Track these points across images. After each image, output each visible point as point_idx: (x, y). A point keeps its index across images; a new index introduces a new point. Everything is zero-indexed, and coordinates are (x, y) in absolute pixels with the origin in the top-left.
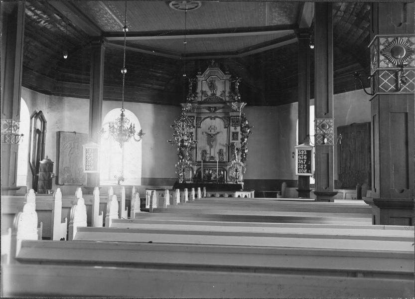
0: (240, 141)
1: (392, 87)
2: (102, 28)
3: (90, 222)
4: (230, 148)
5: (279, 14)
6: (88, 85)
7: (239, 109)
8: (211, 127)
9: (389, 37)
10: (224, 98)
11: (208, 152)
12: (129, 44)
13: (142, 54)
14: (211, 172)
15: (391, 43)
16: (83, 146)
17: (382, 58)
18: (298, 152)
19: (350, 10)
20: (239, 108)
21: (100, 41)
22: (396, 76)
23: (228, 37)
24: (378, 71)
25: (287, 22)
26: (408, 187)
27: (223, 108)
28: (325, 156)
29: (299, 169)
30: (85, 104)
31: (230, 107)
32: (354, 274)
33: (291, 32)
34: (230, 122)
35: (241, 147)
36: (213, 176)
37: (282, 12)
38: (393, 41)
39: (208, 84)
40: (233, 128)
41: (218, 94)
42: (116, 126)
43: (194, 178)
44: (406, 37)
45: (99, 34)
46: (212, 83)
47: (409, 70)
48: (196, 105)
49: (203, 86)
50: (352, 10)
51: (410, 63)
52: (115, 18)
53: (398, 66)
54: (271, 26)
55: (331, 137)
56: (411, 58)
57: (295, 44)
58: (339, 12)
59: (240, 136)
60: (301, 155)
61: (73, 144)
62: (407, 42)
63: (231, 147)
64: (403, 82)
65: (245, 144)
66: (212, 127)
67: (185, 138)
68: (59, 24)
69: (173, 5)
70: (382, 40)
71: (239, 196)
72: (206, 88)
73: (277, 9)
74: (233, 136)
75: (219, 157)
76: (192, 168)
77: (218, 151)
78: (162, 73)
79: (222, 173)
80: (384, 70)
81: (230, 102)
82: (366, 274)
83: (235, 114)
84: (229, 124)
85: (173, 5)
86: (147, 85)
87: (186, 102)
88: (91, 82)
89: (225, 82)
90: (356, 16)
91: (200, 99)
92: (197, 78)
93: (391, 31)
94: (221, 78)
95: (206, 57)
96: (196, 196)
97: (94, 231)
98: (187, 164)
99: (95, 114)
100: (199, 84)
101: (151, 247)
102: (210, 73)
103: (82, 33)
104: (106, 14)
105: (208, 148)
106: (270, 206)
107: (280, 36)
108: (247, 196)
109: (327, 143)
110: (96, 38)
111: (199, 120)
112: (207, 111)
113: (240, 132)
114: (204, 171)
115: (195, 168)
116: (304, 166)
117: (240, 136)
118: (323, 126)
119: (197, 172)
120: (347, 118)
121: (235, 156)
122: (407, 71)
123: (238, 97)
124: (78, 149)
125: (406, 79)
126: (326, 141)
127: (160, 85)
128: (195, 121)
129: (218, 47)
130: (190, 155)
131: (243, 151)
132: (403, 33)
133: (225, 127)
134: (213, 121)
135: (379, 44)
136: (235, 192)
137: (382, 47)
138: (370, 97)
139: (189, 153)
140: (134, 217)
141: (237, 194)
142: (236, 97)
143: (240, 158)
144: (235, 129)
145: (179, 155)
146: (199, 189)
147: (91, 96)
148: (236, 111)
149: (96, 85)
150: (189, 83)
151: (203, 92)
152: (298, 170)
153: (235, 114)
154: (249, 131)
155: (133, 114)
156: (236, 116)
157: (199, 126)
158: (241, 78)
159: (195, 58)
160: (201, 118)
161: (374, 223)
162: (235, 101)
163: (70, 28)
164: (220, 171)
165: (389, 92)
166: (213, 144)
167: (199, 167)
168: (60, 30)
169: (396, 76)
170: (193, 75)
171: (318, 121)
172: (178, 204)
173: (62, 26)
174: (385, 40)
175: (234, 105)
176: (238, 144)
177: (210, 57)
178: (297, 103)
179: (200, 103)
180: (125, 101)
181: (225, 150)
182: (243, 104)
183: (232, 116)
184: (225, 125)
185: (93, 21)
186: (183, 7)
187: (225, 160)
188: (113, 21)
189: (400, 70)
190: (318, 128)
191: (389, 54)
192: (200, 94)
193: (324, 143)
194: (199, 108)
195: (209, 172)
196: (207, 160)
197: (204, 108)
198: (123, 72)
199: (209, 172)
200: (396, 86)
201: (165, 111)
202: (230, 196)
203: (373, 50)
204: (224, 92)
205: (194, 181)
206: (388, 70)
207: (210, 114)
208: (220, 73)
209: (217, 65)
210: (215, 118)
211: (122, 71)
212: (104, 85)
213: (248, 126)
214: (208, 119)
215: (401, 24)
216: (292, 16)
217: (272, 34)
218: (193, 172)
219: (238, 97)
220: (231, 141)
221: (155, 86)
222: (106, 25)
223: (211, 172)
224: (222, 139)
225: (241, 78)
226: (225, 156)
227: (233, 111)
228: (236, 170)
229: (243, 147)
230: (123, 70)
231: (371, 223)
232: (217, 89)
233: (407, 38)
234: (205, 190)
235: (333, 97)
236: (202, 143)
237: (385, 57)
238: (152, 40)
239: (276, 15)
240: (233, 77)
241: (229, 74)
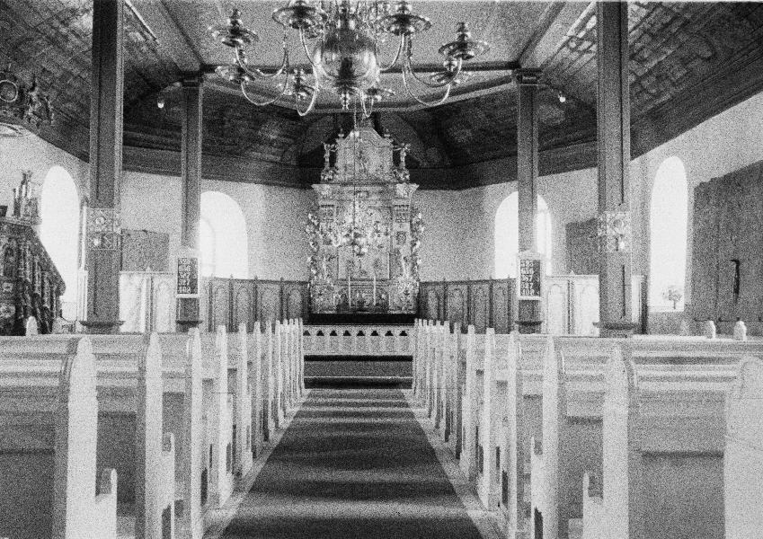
3: (570, 326)
30: (174, 185)
40: (398, 225)
45: (197, 67)
59: (409, 238)
87: (318, 181)
92: (336, 143)
110: (190, 75)
117: (409, 238)
121: (401, 270)
151: (89, 57)
152: (522, 291)
153: (401, 202)
162: (401, 183)
176: (405, 250)
192: (342, 170)
196: (355, 276)
201: (287, 198)
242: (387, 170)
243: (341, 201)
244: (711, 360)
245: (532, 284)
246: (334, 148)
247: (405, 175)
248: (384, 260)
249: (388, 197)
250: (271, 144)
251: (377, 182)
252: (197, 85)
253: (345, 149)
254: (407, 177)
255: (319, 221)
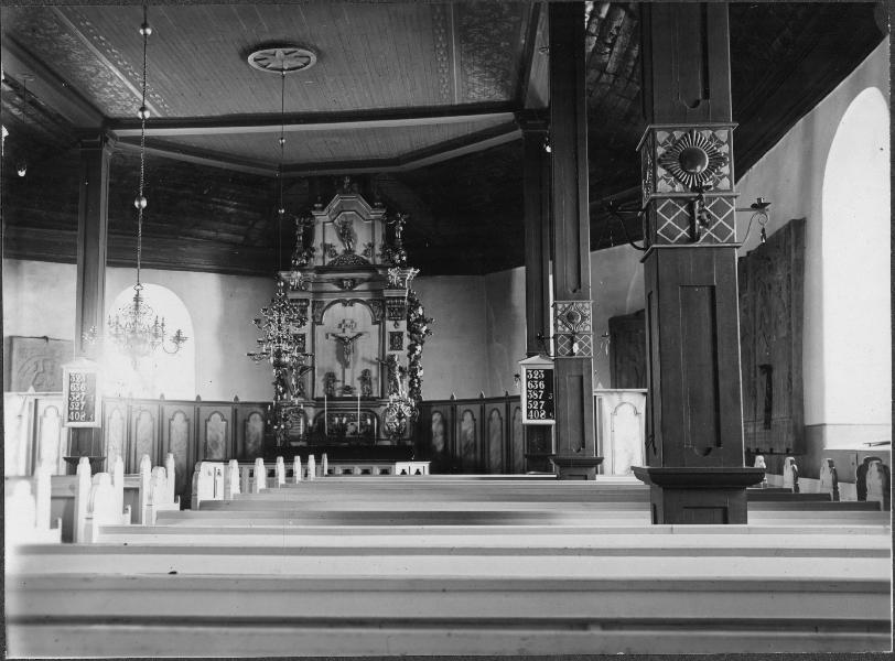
0: (406, 351)
1: (684, 232)
2: (106, 113)
4: (386, 369)
5: (481, 79)
6: (74, 233)
7: (404, 284)
8: (344, 321)
9: (675, 129)
10: (370, 259)
11: (339, 377)
12: (151, 142)
13: (191, 165)
14: (344, 420)
15: (679, 141)
16: (63, 366)
17: (661, 172)
18: (528, 374)
19: (627, 71)
20: (403, 280)
21: (99, 139)
22: (691, 208)
23: (373, 130)
24: (654, 199)
25: (499, 96)
26: (719, 444)
27: (369, 280)
28: (575, 381)
29: (528, 411)
30: (68, 274)
31: (384, 279)
32: (583, 624)
33: (509, 116)
34: (384, 311)
35: (410, 366)
36: (351, 429)
37: (487, 75)
38: (683, 138)
39: (338, 229)
41: (359, 251)
42: (123, 322)
43: (309, 432)
44: (709, 128)
46: (344, 227)
47: (715, 198)
48: (312, 275)
49: (326, 234)
50: (631, 71)
51: (718, 182)
52: (132, 88)
53: (694, 189)
54: (467, 105)
55: (587, 340)
56: (719, 173)
57: (517, 142)
58: (604, 76)
59: (406, 341)
60: (533, 379)
61: (40, 364)
62: (711, 140)
63: (387, 364)
64: (703, 222)
65: (417, 357)
66: (347, 322)
67: (284, 347)
68: (9, 101)
69: (255, 60)
70: (661, 136)
71: (404, 472)
72: (332, 238)
73: (477, 69)
74: (392, 341)
75: (362, 388)
76: (304, 412)
77: (360, 374)
78: (234, 207)
79: (369, 421)
80: (666, 198)
81: (385, 268)
82: (607, 624)
83: (394, 293)
84: (384, 316)
85: (255, 60)
86: (205, 233)
87: (288, 267)
88: (80, 227)
89: (373, 225)
90: (638, 84)
91: (319, 263)
92: (313, 217)
93: (679, 117)
94: (364, 216)
95: (334, 172)
96: (290, 474)
97: (88, 553)
98: (292, 404)
99: (88, 293)
100: (318, 230)
101: (173, 584)
102: (341, 205)
103: (60, 121)
104: (112, 79)
105: (338, 369)
106: (460, 491)
107: (479, 128)
108: (421, 471)
109: (580, 354)
110: (94, 132)
111: (319, 307)
112: (336, 288)
113: (406, 333)
114: (331, 419)
115: (311, 412)
116: (540, 405)
117: (406, 341)
118: (570, 317)
119: (314, 422)
120: (629, 299)
121: (396, 384)
122: (711, 199)
123: (401, 256)
124: (52, 373)
125: (709, 216)
126: (576, 348)
127: (234, 233)
128: (309, 309)
129: (358, 151)
130: (300, 384)
131: (413, 373)
132: (704, 121)
133: (375, 323)
134: (349, 308)
135: (655, 144)
136: (394, 462)
137: (660, 151)
138: (642, 254)
139: (297, 380)
140: (154, 522)
141: (399, 467)
142: (397, 257)
143: (409, 389)
144: (396, 325)
145: (276, 384)
146: (312, 457)
147: (80, 258)
148: (397, 287)
149: (90, 237)
151: (327, 248)
153: (394, 293)
154: (425, 328)
155: (173, 294)
156: (398, 298)
157: (317, 320)
158: (407, 216)
159: (309, 173)
160: (322, 302)
161: (655, 522)
162: (394, 265)
163: (32, 111)
164: (364, 418)
165: (676, 243)
166: (350, 358)
167: (319, 410)
168: (12, 114)
169: (691, 208)
170: (307, 214)
171: (560, 306)
172: (261, 490)
173: (15, 106)
174: (667, 135)
176: (401, 358)
177: (341, 172)
178: (523, 268)
179: (320, 270)
180: (143, 266)
181: (374, 371)
182: (411, 272)
183: (389, 298)
184: (374, 317)
185: (83, 94)
186: (279, 65)
187: (375, 395)
188: (128, 95)
189: (697, 198)
190: (559, 322)
191: (675, 165)
192: (321, 252)
193: (572, 354)
194: (317, 282)
195: (341, 421)
197: (329, 281)
198: (140, 205)
199: (341, 421)
200: (691, 231)
201: (247, 290)
202: (385, 472)
203: (646, 156)
204: (372, 246)
205: (309, 443)
206: (673, 198)
207: (344, 295)
208: (363, 204)
209: (356, 189)
210: (352, 303)
211: (136, 204)
212: (109, 233)
213: (422, 319)
214: (338, 306)
215: (697, 103)
216: (509, 83)
217: (468, 123)
218: (306, 421)
219: (401, 256)
220: (388, 353)
221: (225, 236)
222: (113, 102)
223: (344, 420)
224: (368, 348)
225: (407, 216)
226: (374, 386)
227: (390, 288)
228: (400, 414)
229: (413, 364)
230: (139, 200)
231: (648, 521)
232: (356, 241)
233: (711, 132)
234: (326, 460)
235: (589, 256)
236: (326, 358)
237: (668, 170)
238: (214, 136)
239: (476, 80)
240: (390, 214)
241: (381, 207)
243: (318, 293)
245: (543, 402)
246: (309, 223)
247: (401, 256)
249: (378, 286)
250: (228, 221)
251: (362, 265)
252: (100, 145)
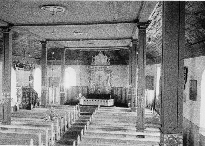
30: (60, 66)
59: (110, 77)
72: (98, 61)
99: (63, 69)
117: (110, 77)
150: (92, 59)
175: (108, 67)
180: (54, 65)
196: (98, 85)
201: (85, 67)
220: (107, 79)
242: (105, 63)
244: (111, 129)
246: (94, 58)
248: (105, 82)
253: (97, 58)
254: (110, 64)
255: (91, 73)
